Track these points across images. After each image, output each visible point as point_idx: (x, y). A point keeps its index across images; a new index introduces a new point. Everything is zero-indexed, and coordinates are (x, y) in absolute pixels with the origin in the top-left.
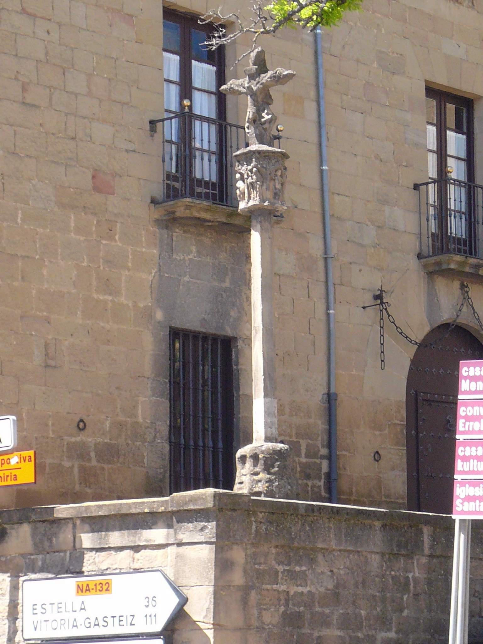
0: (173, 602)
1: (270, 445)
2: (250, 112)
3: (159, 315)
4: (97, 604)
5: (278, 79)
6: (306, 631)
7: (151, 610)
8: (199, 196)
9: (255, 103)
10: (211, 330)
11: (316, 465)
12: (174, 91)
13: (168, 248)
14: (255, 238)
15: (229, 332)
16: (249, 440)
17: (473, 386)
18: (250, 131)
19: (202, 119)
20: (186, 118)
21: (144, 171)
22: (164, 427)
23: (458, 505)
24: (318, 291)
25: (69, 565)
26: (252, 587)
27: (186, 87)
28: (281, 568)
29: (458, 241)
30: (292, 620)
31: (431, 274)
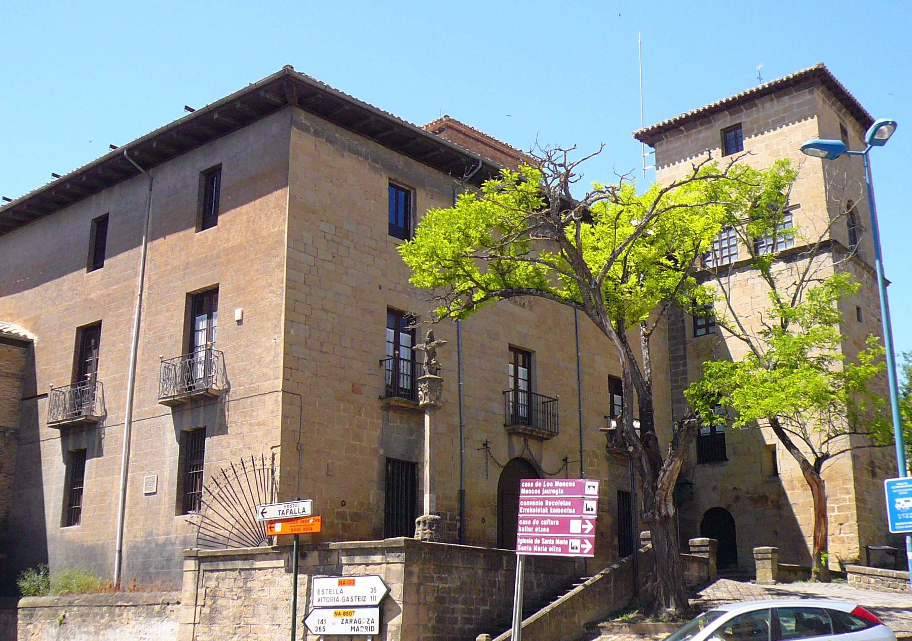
0: (385, 590)
1: (432, 516)
2: (426, 360)
3: (381, 452)
4: (348, 591)
5: (439, 345)
6: (447, 605)
7: (373, 594)
8: (402, 396)
9: (428, 355)
10: (405, 459)
11: (454, 523)
12: (391, 346)
13: (386, 420)
14: (427, 418)
15: (414, 460)
16: (422, 513)
17: (527, 492)
18: (425, 368)
19: (403, 359)
20: (397, 359)
21: (376, 384)
22: (382, 506)
23: (519, 547)
24: (457, 442)
25: (335, 571)
26: (422, 584)
27: (397, 345)
28: (435, 576)
29: (523, 418)
30: (440, 600)
31: (510, 434)
